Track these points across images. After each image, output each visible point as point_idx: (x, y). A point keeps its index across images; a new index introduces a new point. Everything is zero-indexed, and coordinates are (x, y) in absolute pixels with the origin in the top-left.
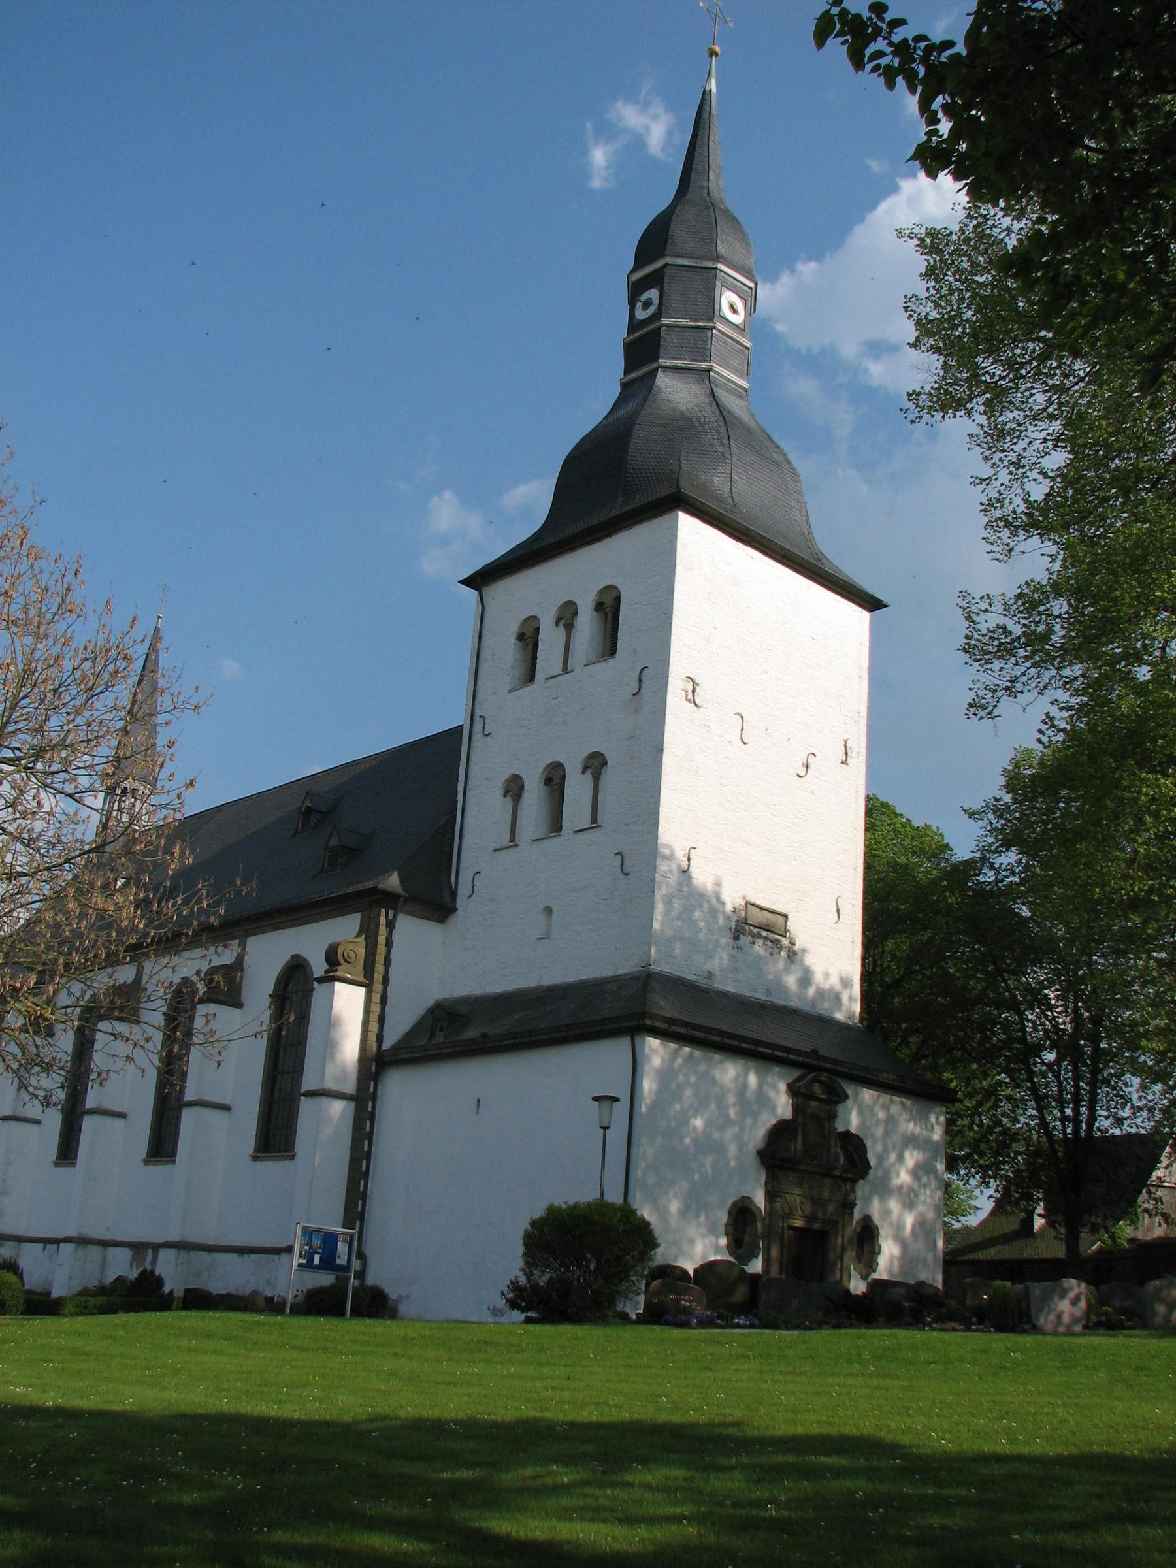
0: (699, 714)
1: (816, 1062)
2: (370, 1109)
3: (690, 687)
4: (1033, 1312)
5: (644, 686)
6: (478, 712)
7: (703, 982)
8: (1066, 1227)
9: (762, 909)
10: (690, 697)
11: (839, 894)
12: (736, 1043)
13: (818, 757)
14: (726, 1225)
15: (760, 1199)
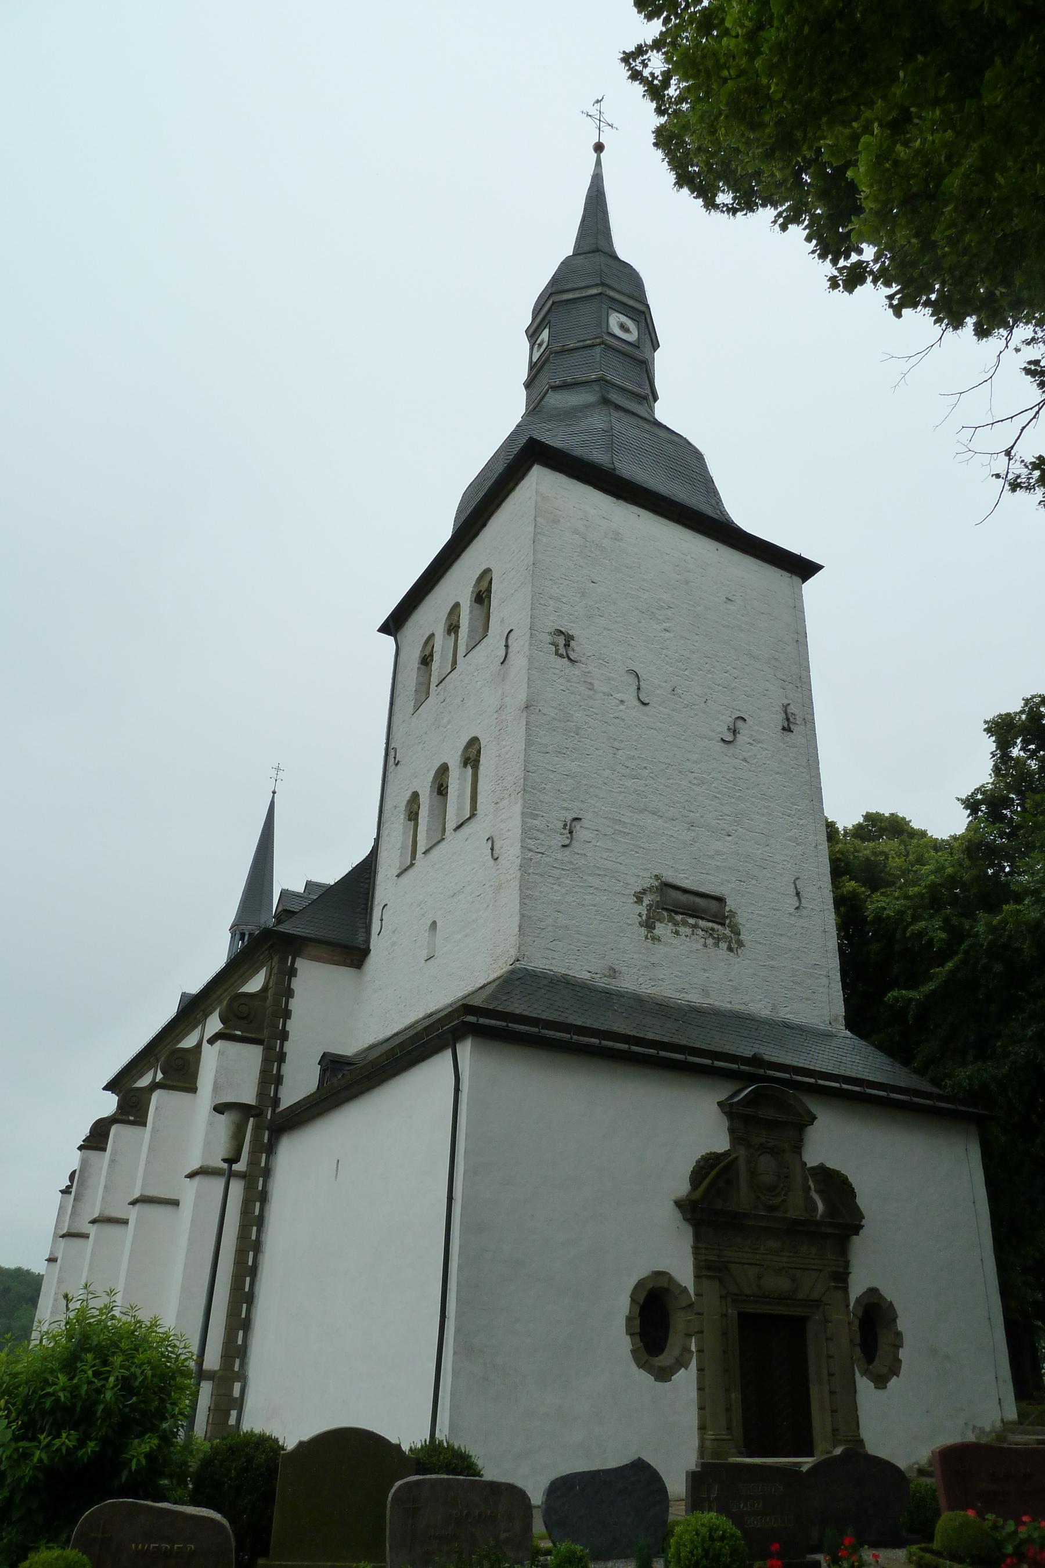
2: (254, 1237)
3: (561, 641)
5: (510, 650)
6: (392, 745)
7: (601, 983)
8: (195, 1485)
9: (685, 891)
10: (562, 651)
12: (625, 1047)
13: (750, 721)
14: (629, 1319)
15: (684, 1274)
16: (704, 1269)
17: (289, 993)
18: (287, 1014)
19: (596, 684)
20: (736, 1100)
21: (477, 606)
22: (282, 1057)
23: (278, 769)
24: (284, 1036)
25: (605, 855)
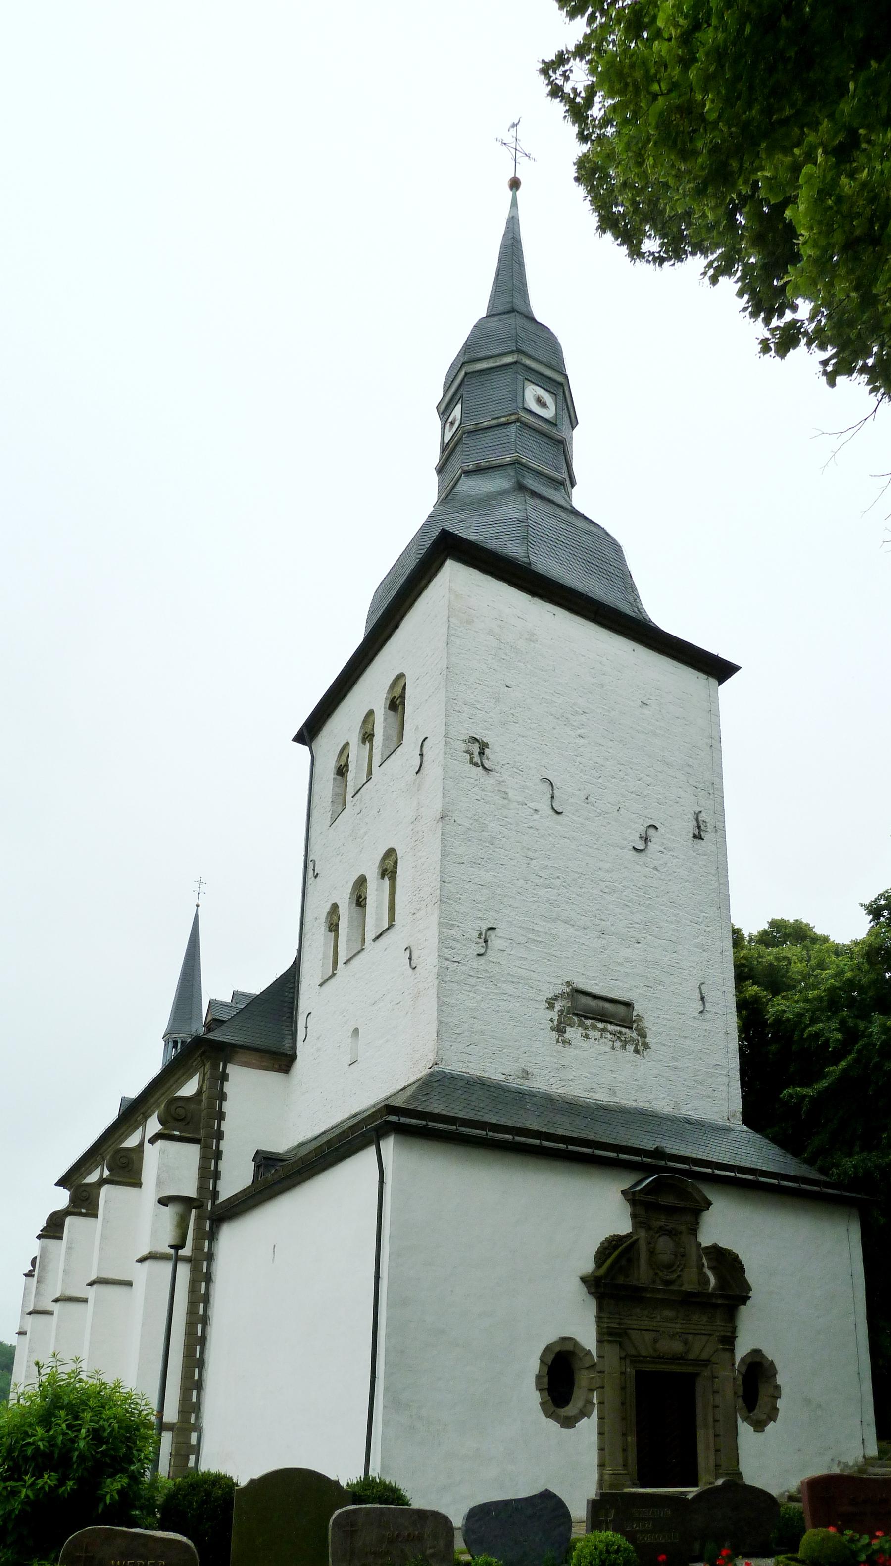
0: (489, 781)
1: (663, 1163)
3: (476, 749)
4: (740, 1482)
5: (425, 758)
6: (311, 858)
10: (477, 759)
11: (703, 980)
13: (661, 829)
16: (605, 1335)
17: (223, 1097)
18: (221, 1116)
19: (511, 794)
20: (639, 1188)
21: (391, 713)
22: (218, 1155)
23: (201, 882)
24: (220, 1136)
25: (518, 963)
